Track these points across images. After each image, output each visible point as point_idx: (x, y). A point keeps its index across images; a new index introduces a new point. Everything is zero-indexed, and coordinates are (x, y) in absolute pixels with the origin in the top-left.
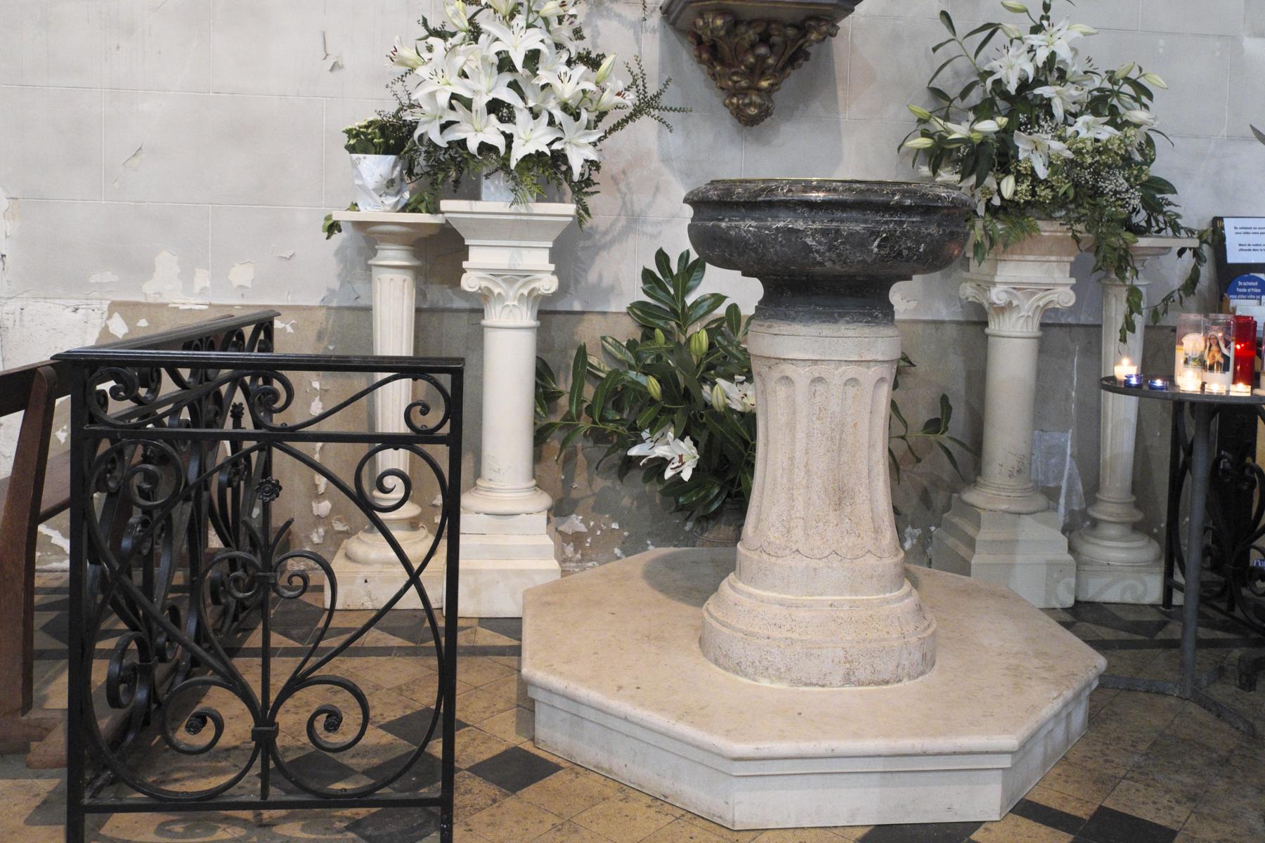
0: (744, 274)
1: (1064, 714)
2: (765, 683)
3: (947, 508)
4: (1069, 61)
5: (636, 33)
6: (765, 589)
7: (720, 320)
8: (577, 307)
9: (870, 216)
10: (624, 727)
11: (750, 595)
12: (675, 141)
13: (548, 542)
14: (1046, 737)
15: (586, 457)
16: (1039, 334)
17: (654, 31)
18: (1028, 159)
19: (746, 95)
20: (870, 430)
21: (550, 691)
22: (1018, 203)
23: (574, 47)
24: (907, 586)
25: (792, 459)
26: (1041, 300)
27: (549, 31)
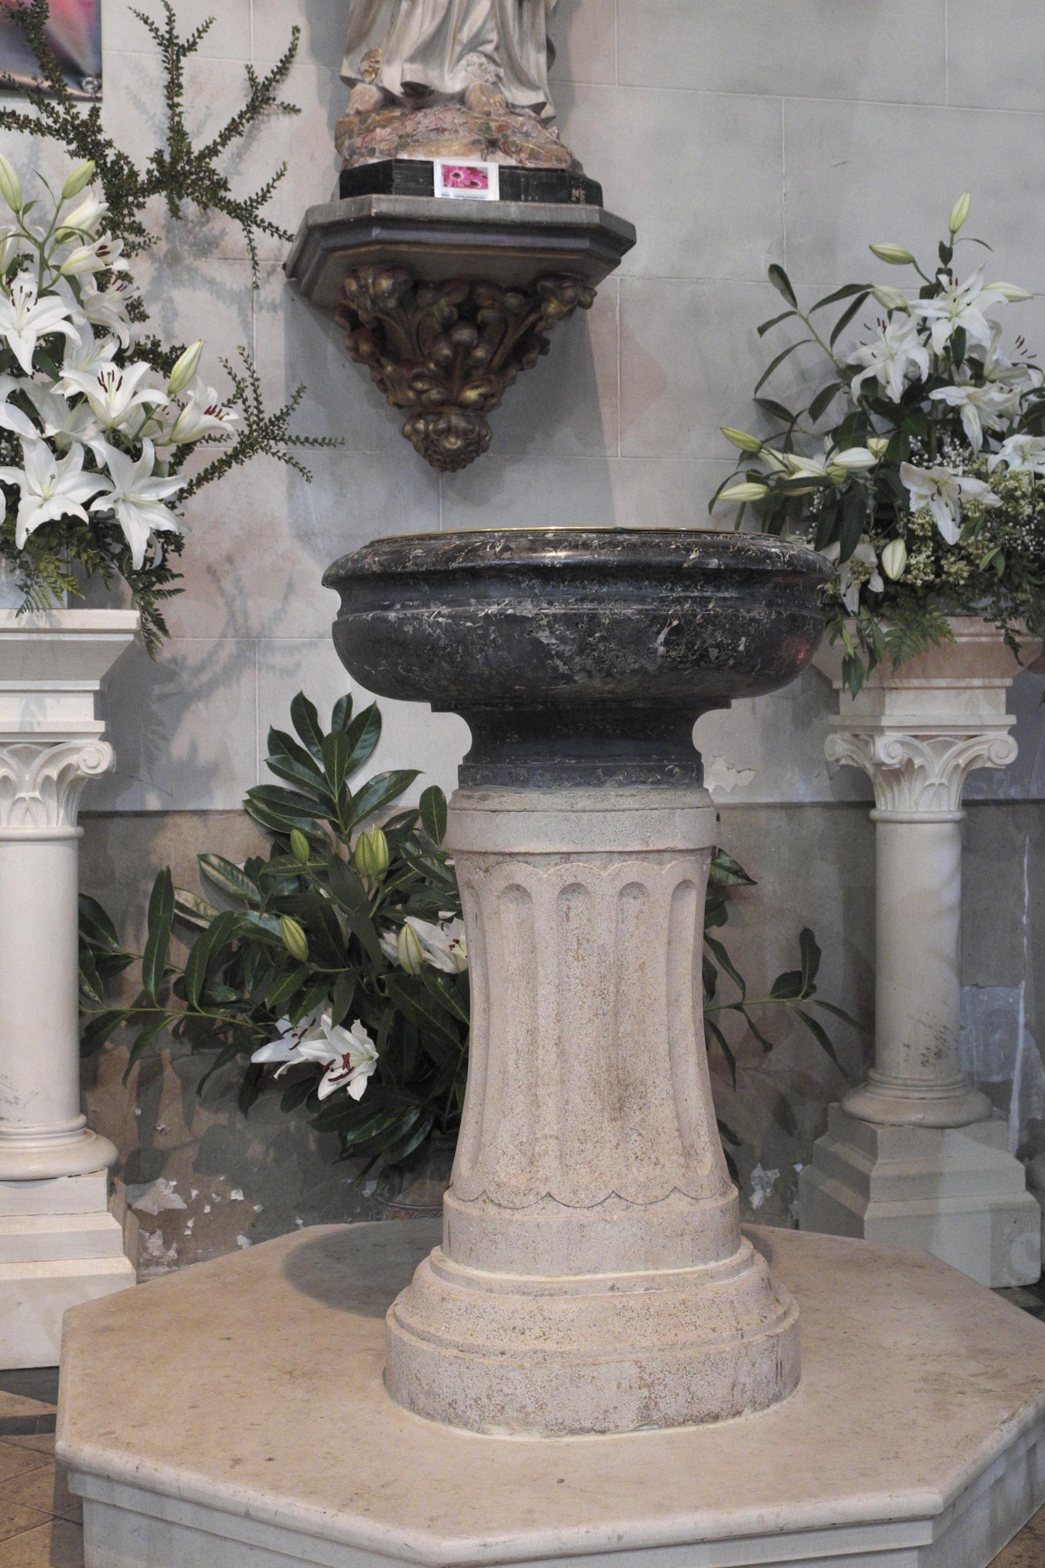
0: (435, 709)
1: (1022, 1450)
2: (499, 1434)
3: (821, 1130)
4: (987, 344)
5: (241, 312)
6: (494, 1268)
7: (410, 815)
8: (153, 803)
9: (648, 589)
10: (244, 1530)
11: (469, 1281)
12: (318, 499)
13: (112, 1224)
14: (993, 1487)
15: (180, 1076)
16: (958, 815)
17: (274, 307)
18: (927, 512)
19: (440, 415)
20: (669, 973)
21: (108, 1478)
22: (912, 587)
23: (128, 333)
24: (746, 1249)
25: (532, 1033)
26: (959, 755)
27: (81, 303)
